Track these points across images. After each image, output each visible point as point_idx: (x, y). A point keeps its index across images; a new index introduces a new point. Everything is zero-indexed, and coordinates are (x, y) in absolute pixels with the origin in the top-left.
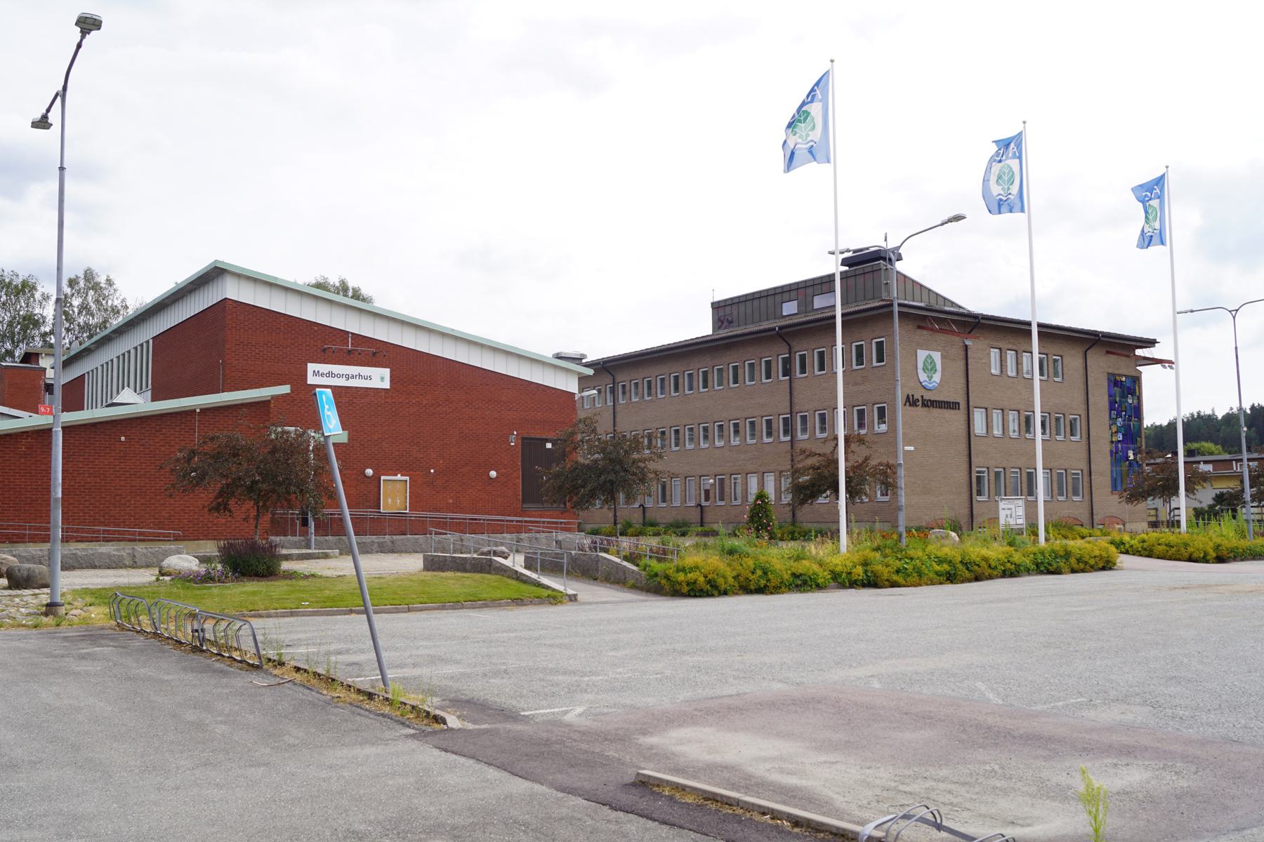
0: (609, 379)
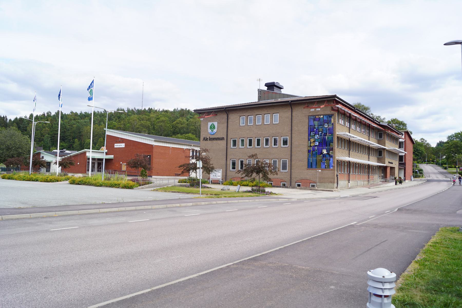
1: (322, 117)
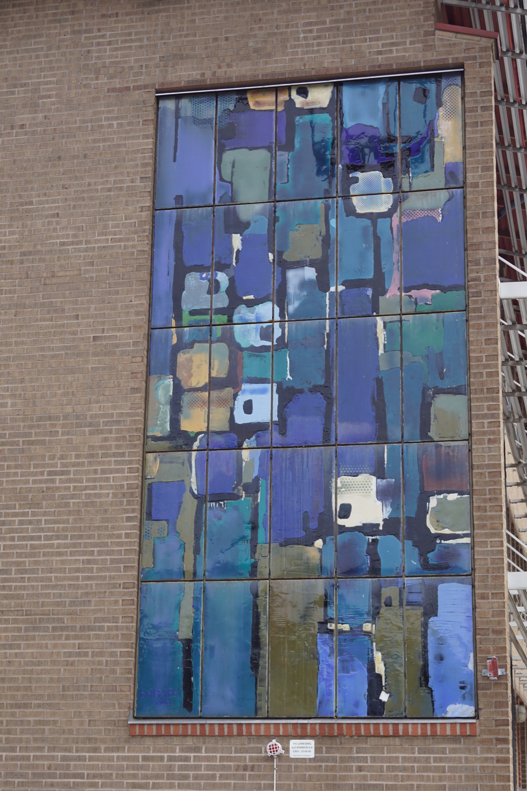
1: (321, 96)
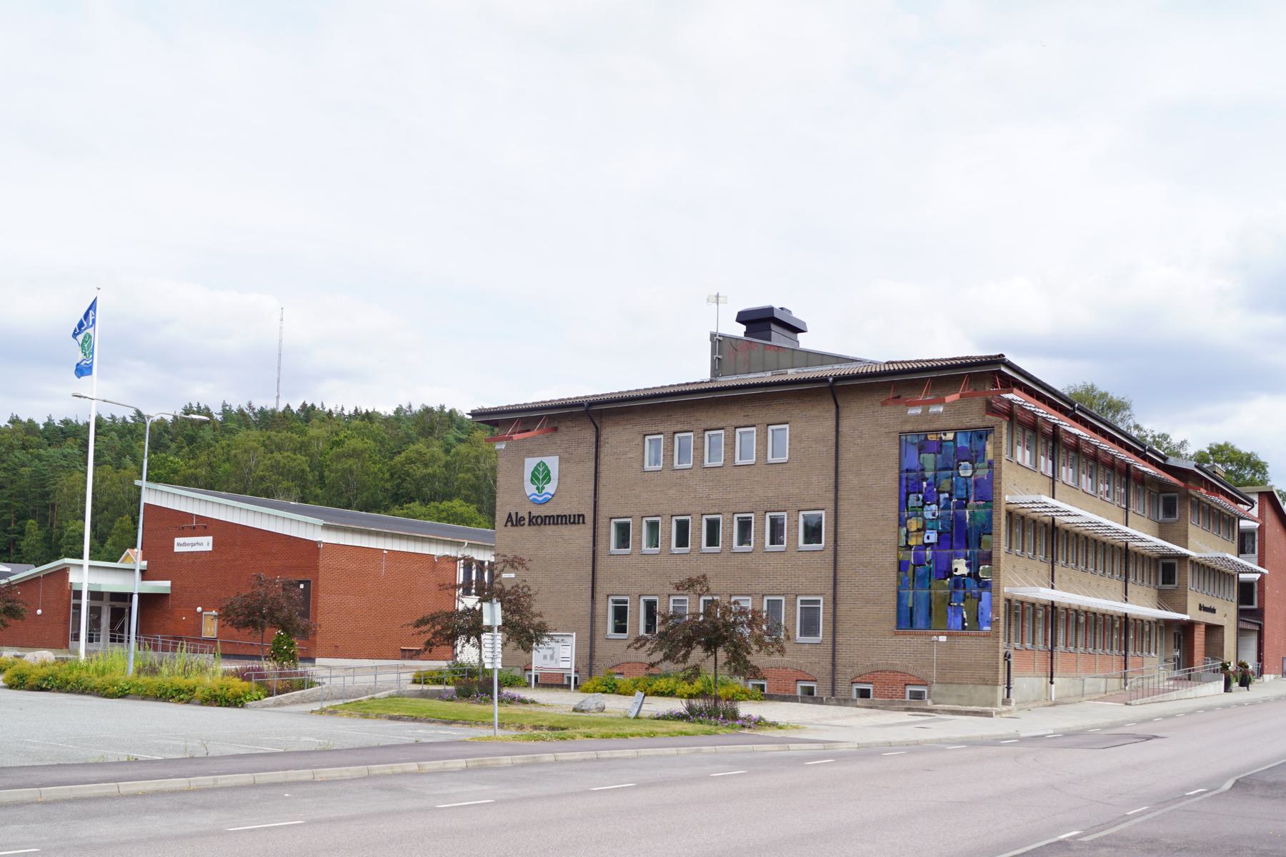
0: (588, 434)
1: (950, 436)
